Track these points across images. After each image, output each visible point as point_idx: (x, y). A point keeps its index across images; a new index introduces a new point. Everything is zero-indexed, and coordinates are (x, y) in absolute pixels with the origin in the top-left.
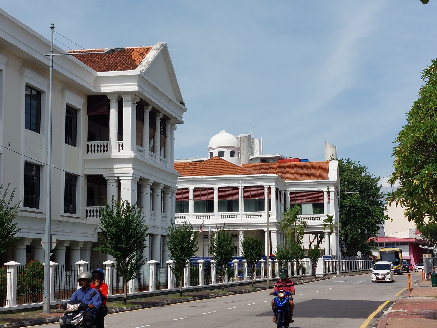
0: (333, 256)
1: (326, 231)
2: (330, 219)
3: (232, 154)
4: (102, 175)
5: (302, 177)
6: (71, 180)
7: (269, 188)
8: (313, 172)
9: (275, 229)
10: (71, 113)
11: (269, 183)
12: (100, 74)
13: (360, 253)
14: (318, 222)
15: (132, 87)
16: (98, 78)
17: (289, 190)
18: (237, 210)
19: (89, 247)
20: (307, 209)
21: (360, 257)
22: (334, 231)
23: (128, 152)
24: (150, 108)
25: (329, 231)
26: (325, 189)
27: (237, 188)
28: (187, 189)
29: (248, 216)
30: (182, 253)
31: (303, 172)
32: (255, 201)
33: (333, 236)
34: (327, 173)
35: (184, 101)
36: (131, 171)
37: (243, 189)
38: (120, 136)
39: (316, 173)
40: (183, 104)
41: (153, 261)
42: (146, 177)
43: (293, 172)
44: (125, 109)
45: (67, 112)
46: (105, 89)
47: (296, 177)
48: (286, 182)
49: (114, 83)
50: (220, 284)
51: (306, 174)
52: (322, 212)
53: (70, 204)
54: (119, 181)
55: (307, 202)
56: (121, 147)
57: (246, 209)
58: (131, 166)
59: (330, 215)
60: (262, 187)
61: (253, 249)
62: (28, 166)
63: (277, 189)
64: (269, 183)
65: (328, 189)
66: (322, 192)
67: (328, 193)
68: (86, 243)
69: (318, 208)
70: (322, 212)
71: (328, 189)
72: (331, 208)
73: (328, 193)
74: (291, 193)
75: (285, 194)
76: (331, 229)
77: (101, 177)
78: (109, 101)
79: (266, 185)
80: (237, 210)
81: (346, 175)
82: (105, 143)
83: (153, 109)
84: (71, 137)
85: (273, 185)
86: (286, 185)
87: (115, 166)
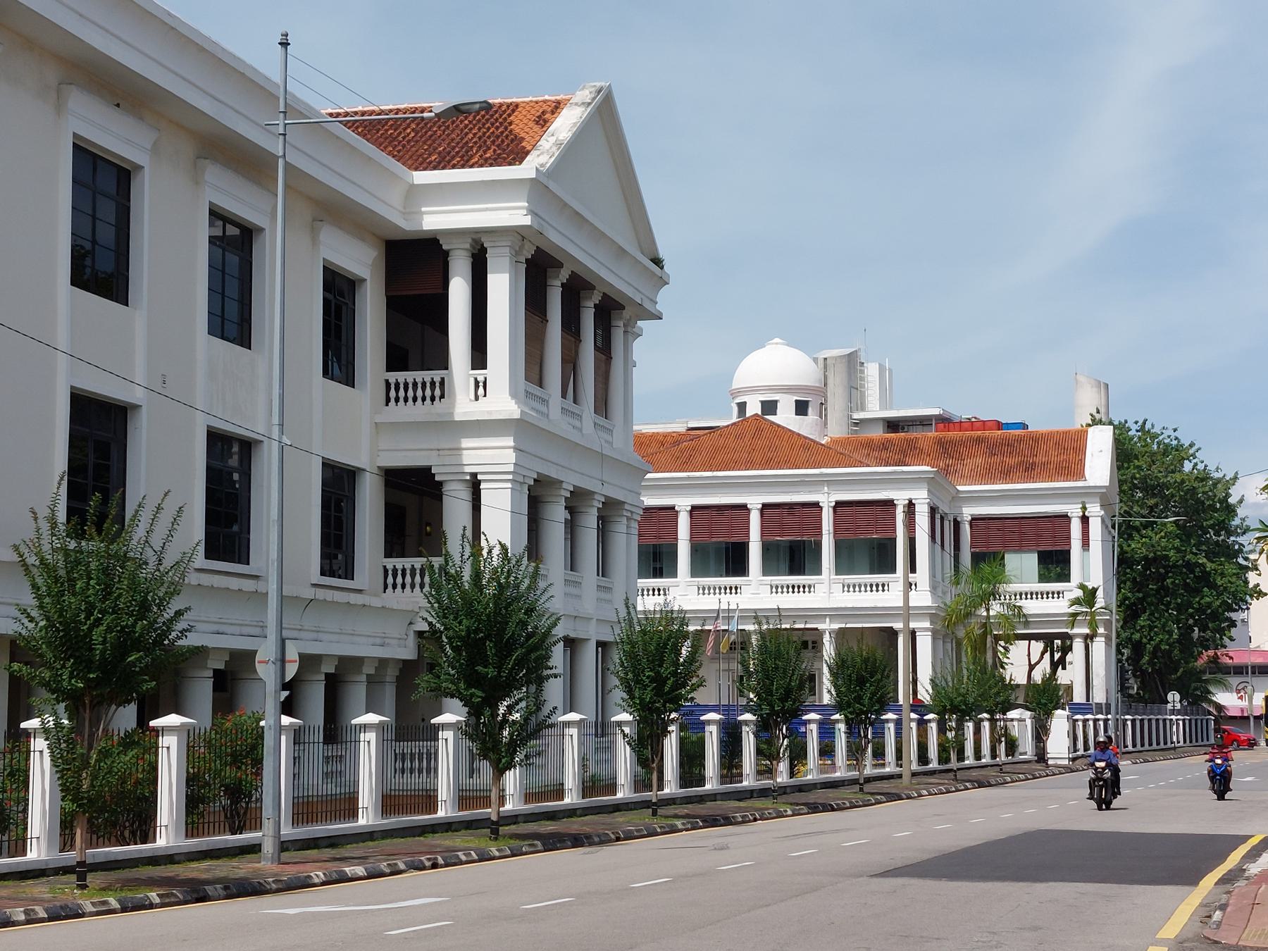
1: (1076, 631)
3: (801, 408)
5: (1006, 474)
6: (339, 484)
7: (911, 506)
8: (1040, 459)
9: (927, 624)
10: (339, 292)
11: (908, 490)
12: (422, 177)
14: (1051, 604)
16: (413, 189)
17: (968, 512)
19: (391, 674)
20: (1022, 567)
21: (1178, 706)
22: (1101, 630)
23: (501, 401)
24: (564, 275)
25: (1087, 631)
26: (1074, 510)
27: (816, 505)
29: (847, 587)
30: (658, 692)
32: (870, 543)
33: (1099, 647)
34: (1081, 463)
35: (662, 254)
36: (510, 457)
37: (835, 508)
38: (479, 357)
40: (658, 262)
41: (573, 716)
42: (553, 473)
43: (979, 460)
44: (491, 278)
45: (328, 287)
46: (435, 219)
47: (989, 475)
48: (960, 488)
49: (459, 203)
51: (1020, 464)
52: (1065, 576)
53: (337, 551)
54: (475, 485)
55: (1020, 548)
56: (480, 387)
57: (698, 569)
58: (510, 442)
59: (1090, 585)
60: (890, 504)
61: (861, 682)
62: (218, 441)
63: (933, 511)
64: (908, 490)
65: (1084, 508)
66: (1065, 518)
67: (1085, 520)
68: (383, 663)
69: (1055, 564)
70: (1065, 576)
71: (1084, 508)
72: (1092, 565)
73: (1085, 520)
74: (975, 520)
75: (957, 525)
76: (1093, 625)
78: (446, 254)
79: (900, 497)
80: (817, 571)
82: (437, 375)
83: (574, 276)
84: (339, 359)
85: (921, 497)
86: (958, 499)
87: (466, 443)
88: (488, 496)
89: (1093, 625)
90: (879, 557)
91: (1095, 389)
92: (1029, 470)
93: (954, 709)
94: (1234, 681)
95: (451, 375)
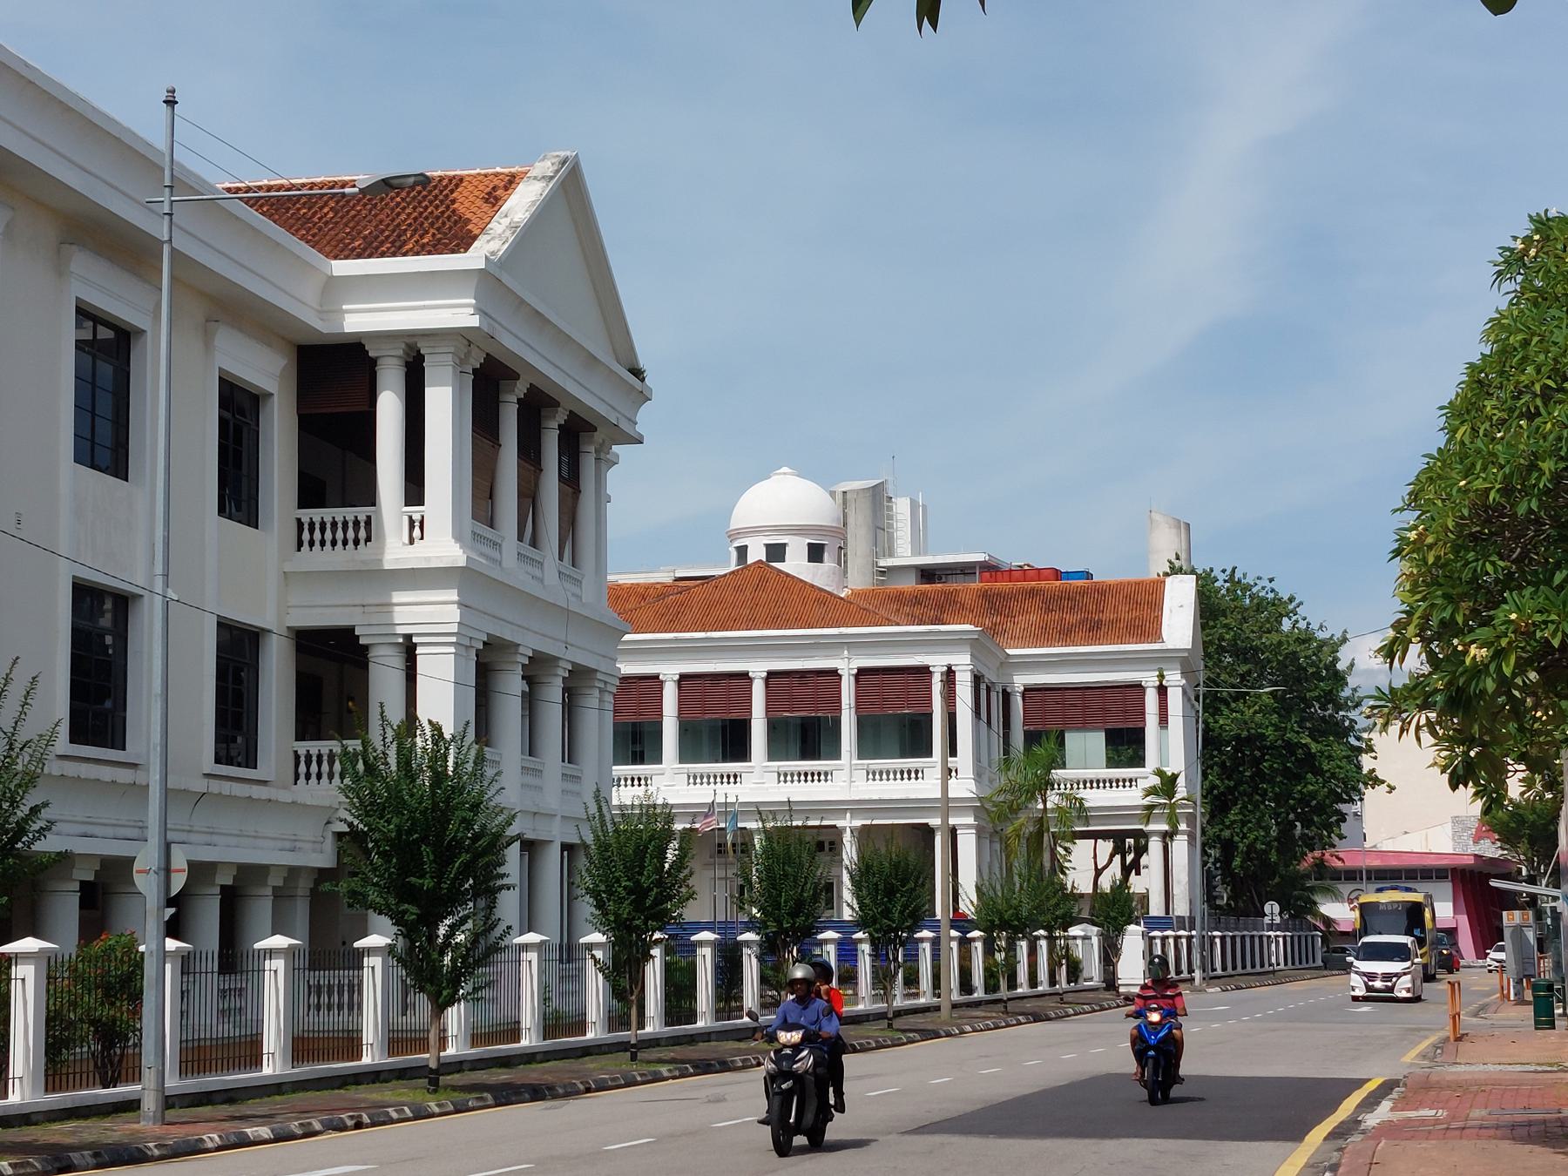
0: (1181, 919)
1: (1152, 827)
2: (1168, 784)
3: (815, 553)
4: (351, 630)
5: (1066, 634)
6: (238, 649)
7: (950, 674)
8: (1108, 615)
9: (970, 820)
10: (238, 408)
11: (948, 655)
12: (343, 267)
13: (1277, 908)
14: (1121, 794)
15: (458, 313)
16: (332, 280)
17: (1020, 681)
18: (836, 755)
19: (304, 886)
20: (1085, 749)
21: (1278, 920)
22: (1183, 827)
23: (442, 545)
24: (521, 389)
25: (1165, 827)
26: (1149, 679)
27: (834, 673)
28: (656, 677)
29: (872, 774)
30: (638, 906)
31: (1072, 618)
32: (900, 722)
34: (1157, 621)
35: (643, 362)
36: (454, 614)
38: (414, 490)
39: (1119, 620)
40: (638, 373)
41: (532, 937)
43: (1033, 618)
44: (430, 393)
45: (224, 403)
46: (358, 320)
47: (1044, 635)
48: (1009, 651)
49: (385, 298)
50: (623, 1035)
51: (1082, 622)
52: (1138, 760)
54: (409, 650)
55: (1084, 725)
56: (416, 527)
57: (688, 752)
58: (453, 595)
59: (1169, 771)
60: (925, 671)
61: (890, 892)
63: (977, 679)
64: (948, 655)
65: (1161, 676)
66: (1138, 688)
67: (1162, 691)
68: (293, 872)
69: (1126, 745)
70: (1138, 760)
71: (1161, 676)
72: (1170, 746)
73: (1162, 691)
74: (1028, 691)
75: (1007, 696)
76: (1173, 820)
77: (345, 636)
78: (373, 362)
79: (937, 662)
80: (836, 755)
81: (1226, 626)
82: (361, 512)
84: (238, 495)
85: (962, 662)
87: (398, 597)
88: (426, 663)
89: (1173, 820)
90: (912, 737)
91: (1174, 531)
92: (1094, 630)
93: (1004, 925)
94: (1345, 888)
95: (379, 513)
